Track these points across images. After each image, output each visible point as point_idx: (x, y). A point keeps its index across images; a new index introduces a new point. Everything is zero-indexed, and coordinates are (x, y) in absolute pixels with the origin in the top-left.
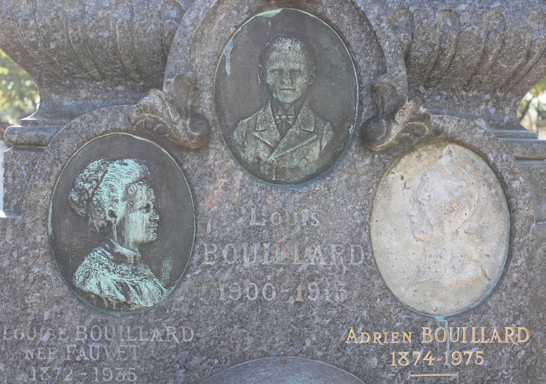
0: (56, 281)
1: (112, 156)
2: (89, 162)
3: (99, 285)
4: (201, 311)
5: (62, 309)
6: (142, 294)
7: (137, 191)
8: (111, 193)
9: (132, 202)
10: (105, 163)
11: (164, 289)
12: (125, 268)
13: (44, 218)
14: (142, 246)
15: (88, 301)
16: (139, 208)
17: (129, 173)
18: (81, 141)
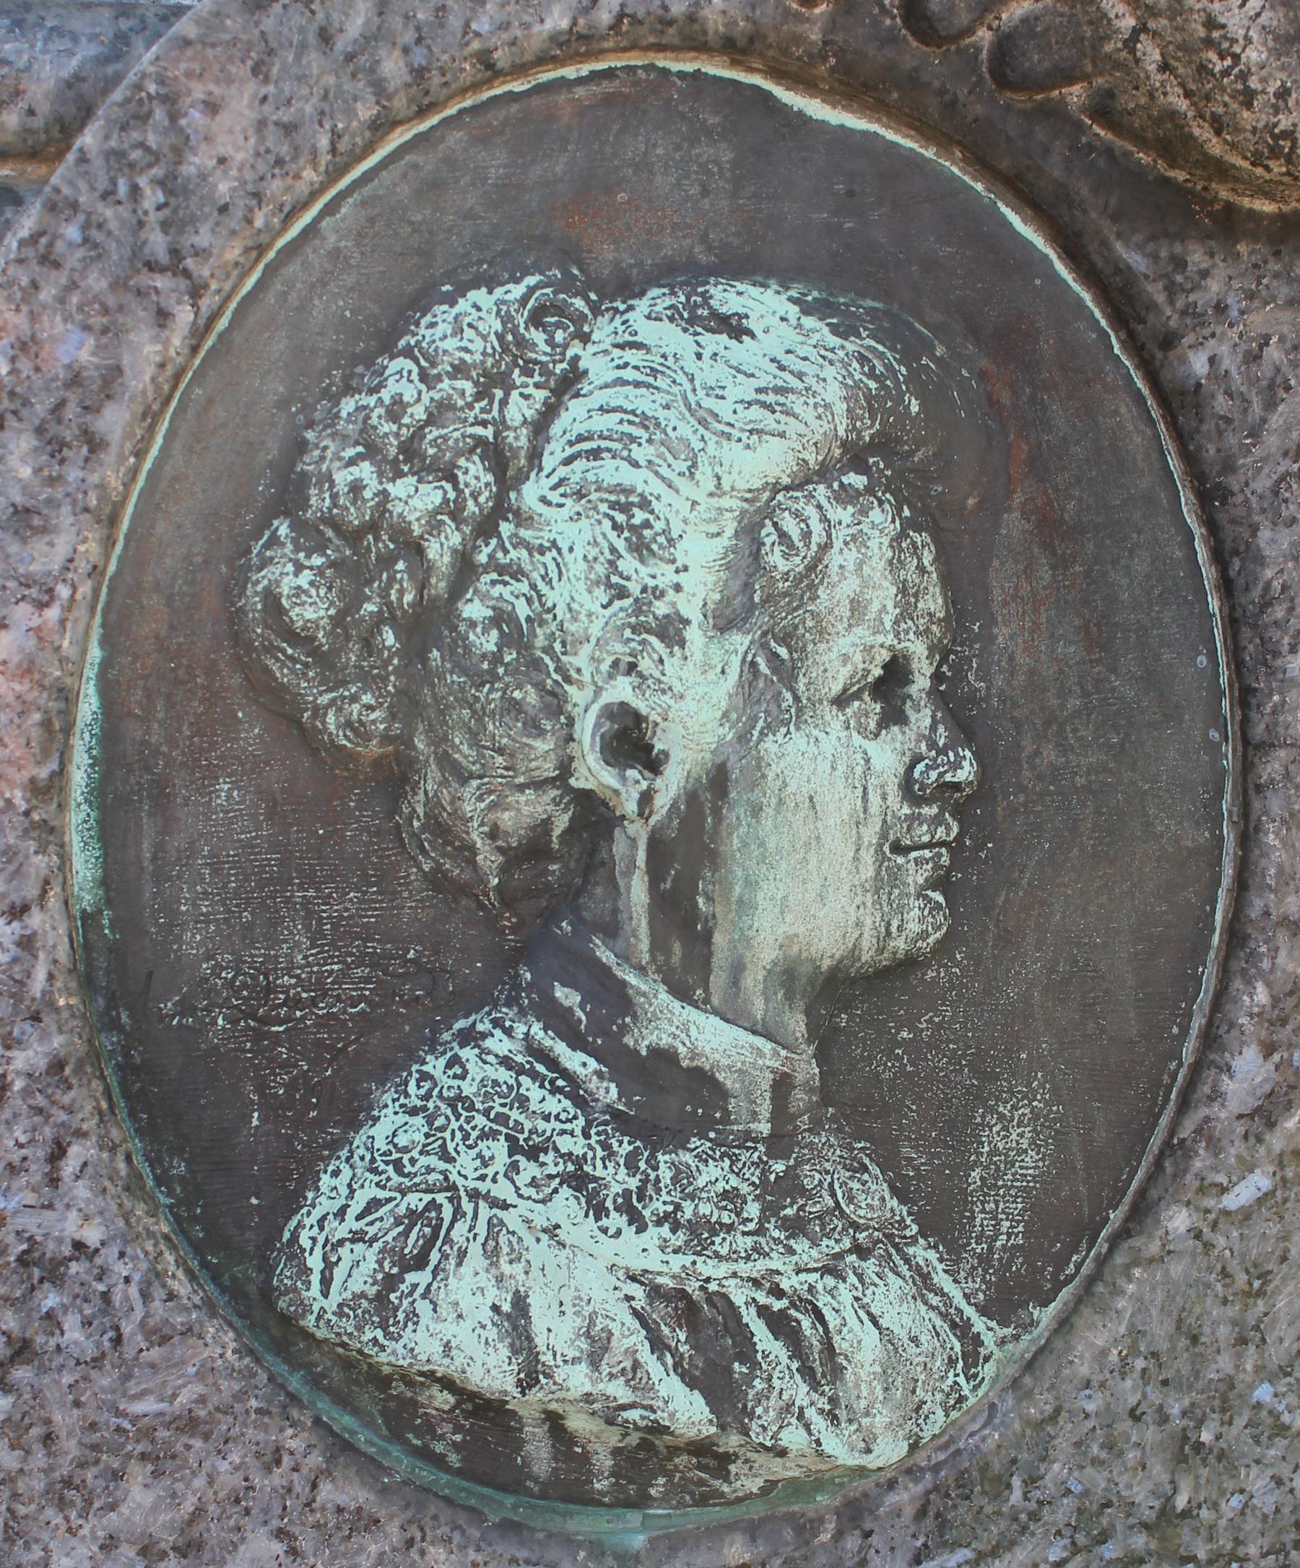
0: (146, 1296)
1: (607, 252)
2: (422, 301)
3: (515, 1320)
4: (1257, 1481)
5: (199, 1512)
6: (837, 1372)
7: (825, 547)
8: (628, 563)
9: (785, 640)
10: (560, 310)
11: (979, 1324)
12: (713, 1175)
13: (43, 773)
14: (841, 998)
15: (396, 1436)
16: (837, 688)
17: (773, 398)
18: (366, 111)
